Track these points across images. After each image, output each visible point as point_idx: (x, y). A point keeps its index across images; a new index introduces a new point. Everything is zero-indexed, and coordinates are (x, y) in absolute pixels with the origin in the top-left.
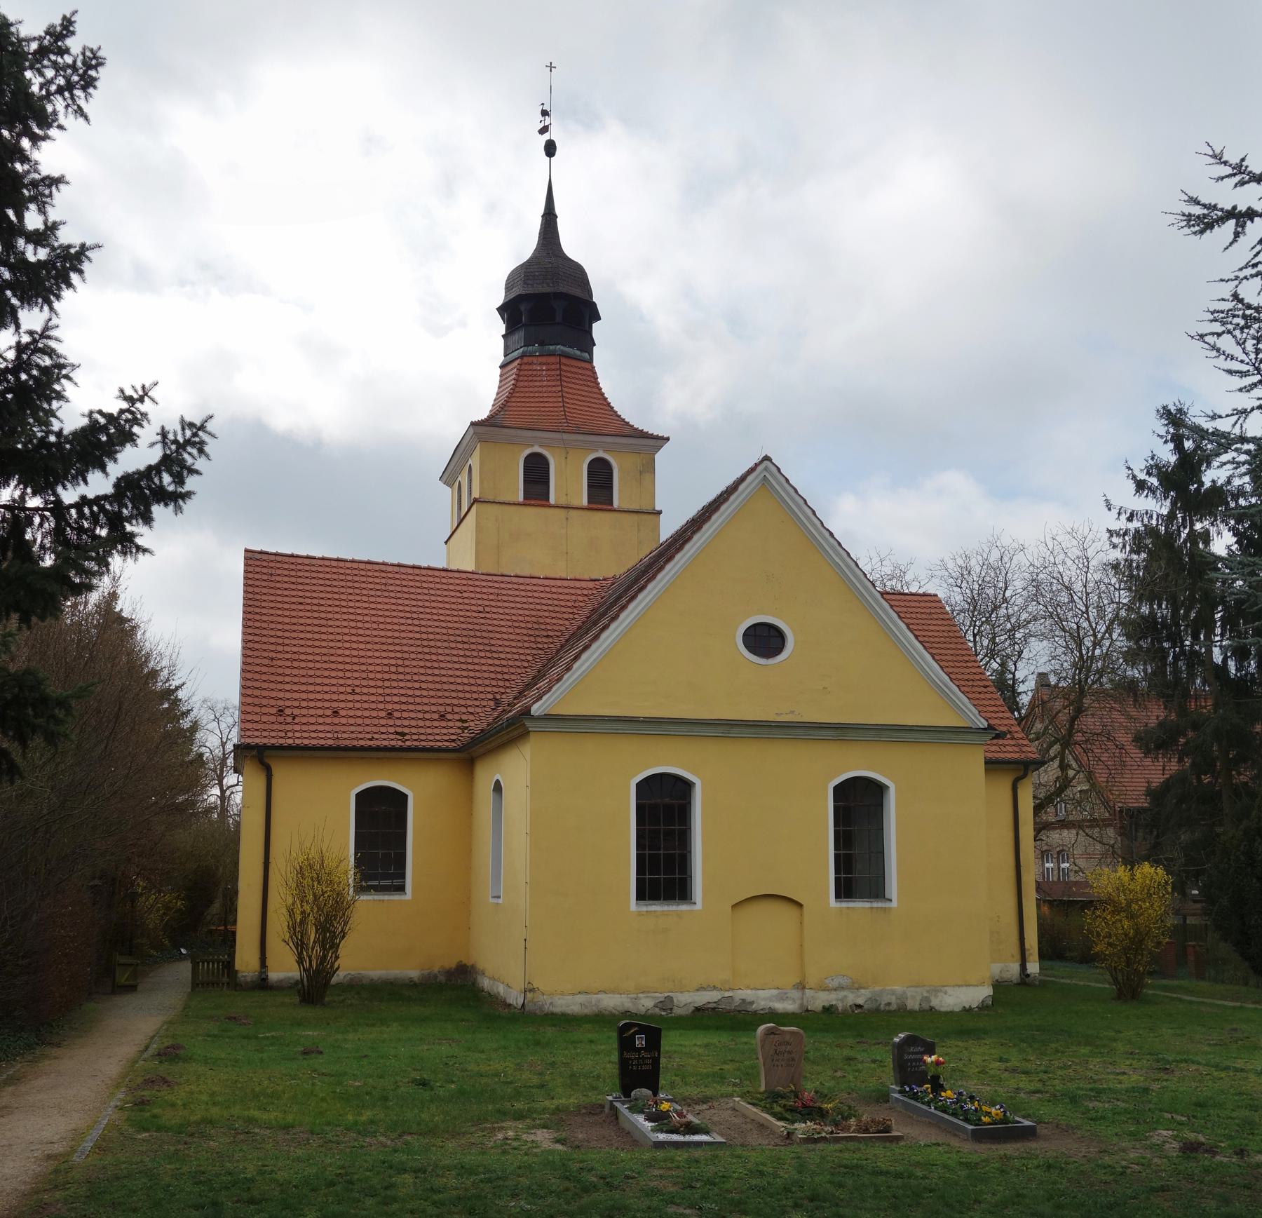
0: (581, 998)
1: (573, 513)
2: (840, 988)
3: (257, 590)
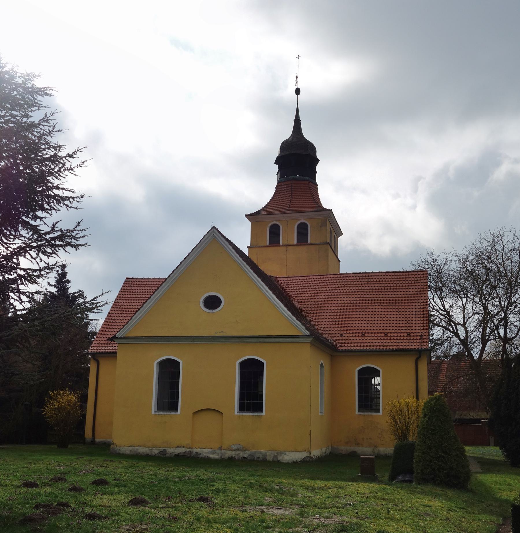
0: (130, 448)
1: (289, 248)
2: (238, 450)
3: (380, 285)
